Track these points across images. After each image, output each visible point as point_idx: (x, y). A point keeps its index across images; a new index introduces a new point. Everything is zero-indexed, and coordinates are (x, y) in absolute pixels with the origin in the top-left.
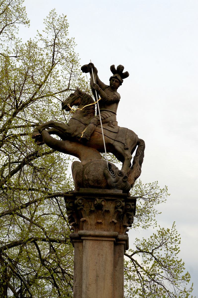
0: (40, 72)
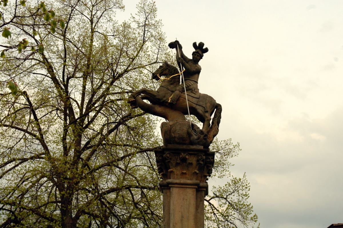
0: (133, 48)
